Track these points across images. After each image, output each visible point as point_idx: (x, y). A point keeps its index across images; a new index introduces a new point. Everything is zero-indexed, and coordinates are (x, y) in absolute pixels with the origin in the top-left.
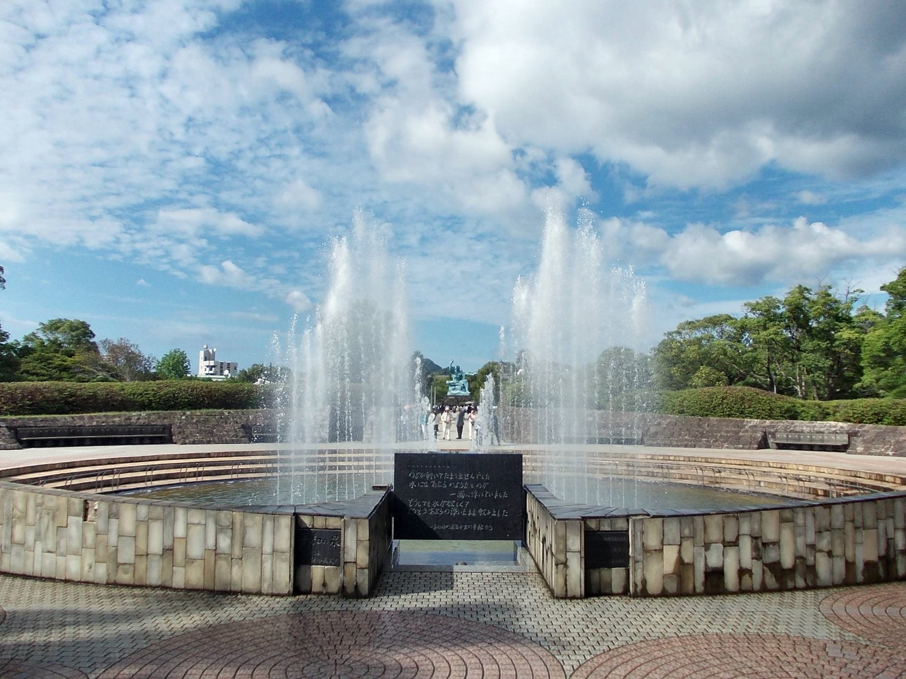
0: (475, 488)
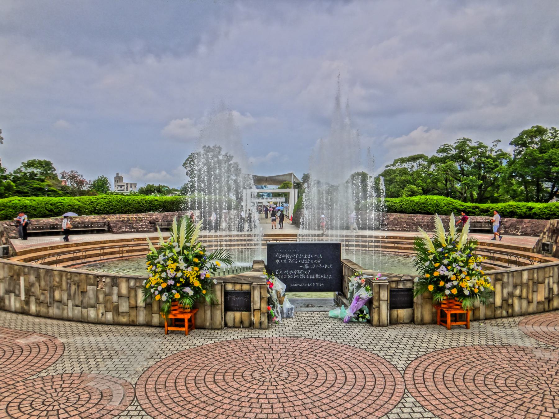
0: (314, 263)
